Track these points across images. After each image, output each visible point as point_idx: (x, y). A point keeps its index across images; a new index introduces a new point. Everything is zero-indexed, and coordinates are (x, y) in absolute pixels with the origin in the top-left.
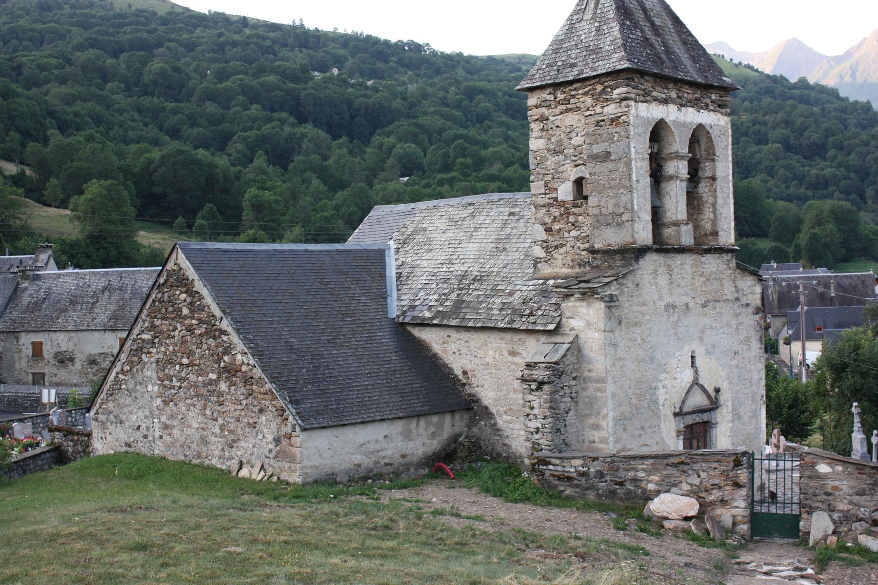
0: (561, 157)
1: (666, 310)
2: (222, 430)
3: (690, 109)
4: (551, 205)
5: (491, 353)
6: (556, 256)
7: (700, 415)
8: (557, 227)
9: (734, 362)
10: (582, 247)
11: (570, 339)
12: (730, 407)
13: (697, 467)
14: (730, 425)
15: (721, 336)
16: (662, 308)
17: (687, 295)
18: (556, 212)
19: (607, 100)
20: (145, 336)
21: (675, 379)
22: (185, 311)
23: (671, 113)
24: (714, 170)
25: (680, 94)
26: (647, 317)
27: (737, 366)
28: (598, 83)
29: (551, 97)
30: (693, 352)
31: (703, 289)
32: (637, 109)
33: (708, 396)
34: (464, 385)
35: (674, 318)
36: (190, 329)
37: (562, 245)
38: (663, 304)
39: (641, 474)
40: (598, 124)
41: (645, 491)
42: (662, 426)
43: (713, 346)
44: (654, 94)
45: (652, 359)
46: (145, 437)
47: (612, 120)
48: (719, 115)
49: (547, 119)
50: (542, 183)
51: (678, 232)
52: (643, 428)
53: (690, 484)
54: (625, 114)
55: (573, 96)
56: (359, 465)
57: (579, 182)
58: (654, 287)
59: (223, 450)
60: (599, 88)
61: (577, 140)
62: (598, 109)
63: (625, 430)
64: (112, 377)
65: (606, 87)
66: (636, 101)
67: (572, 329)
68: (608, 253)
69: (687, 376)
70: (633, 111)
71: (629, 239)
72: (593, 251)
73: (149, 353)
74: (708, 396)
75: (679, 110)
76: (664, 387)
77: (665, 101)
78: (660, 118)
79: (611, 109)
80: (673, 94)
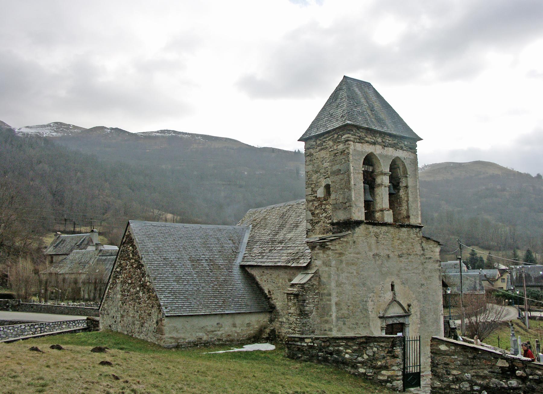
0: (319, 174)
1: (374, 258)
2: (140, 317)
3: (390, 148)
4: (314, 200)
5: (281, 280)
6: (316, 228)
7: (397, 318)
8: (317, 212)
9: (421, 290)
10: (328, 222)
11: (313, 271)
12: (419, 316)
13: (372, 345)
14: (419, 326)
15: (412, 274)
16: (371, 256)
17: (389, 250)
18: (316, 204)
19: (339, 142)
20: (118, 270)
21: (380, 297)
22: (131, 256)
23: (377, 150)
24: (407, 182)
25: (384, 140)
26: (361, 261)
27: (423, 292)
28: (335, 133)
29: (314, 143)
30: (393, 282)
31: (400, 247)
32: (355, 146)
33: (403, 308)
34: (269, 298)
35: (379, 262)
36: (132, 265)
37: (319, 222)
38: (372, 254)
39: (341, 348)
40: (335, 155)
41: (344, 358)
42: (371, 323)
43: (407, 280)
44: (366, 139)
45: (364, 284)
46: (115, 322)
47: (342, 153)
48: (410, 153)
49: (313, 155)
50: (310, 189)
51: (383, 215)
52: (357, 324)
53: (368, 355)
54: (347, 148)
55: (324, 142)
56: (201, 339)
57: (328, 187)
58: (366, 244)
59: (139, 328)
60: (336, 136)
61: (326, 165)
62: (335, 147)
63: (344, 324)
64: (107, 292)
65: (339, 135)
66: (354, 142)
67: (316, 266)
68: (338, 224)
69: (389, 295)
70: (352, 147)
71: (349, 216)
72: (332, 224)
73: (119, 278)
74: (403, 308)
75: (383, 148)
76: (372, 301)
77: (374, 143)
78: (370, 152)
79: (341, 147)
80: (379, 140)
